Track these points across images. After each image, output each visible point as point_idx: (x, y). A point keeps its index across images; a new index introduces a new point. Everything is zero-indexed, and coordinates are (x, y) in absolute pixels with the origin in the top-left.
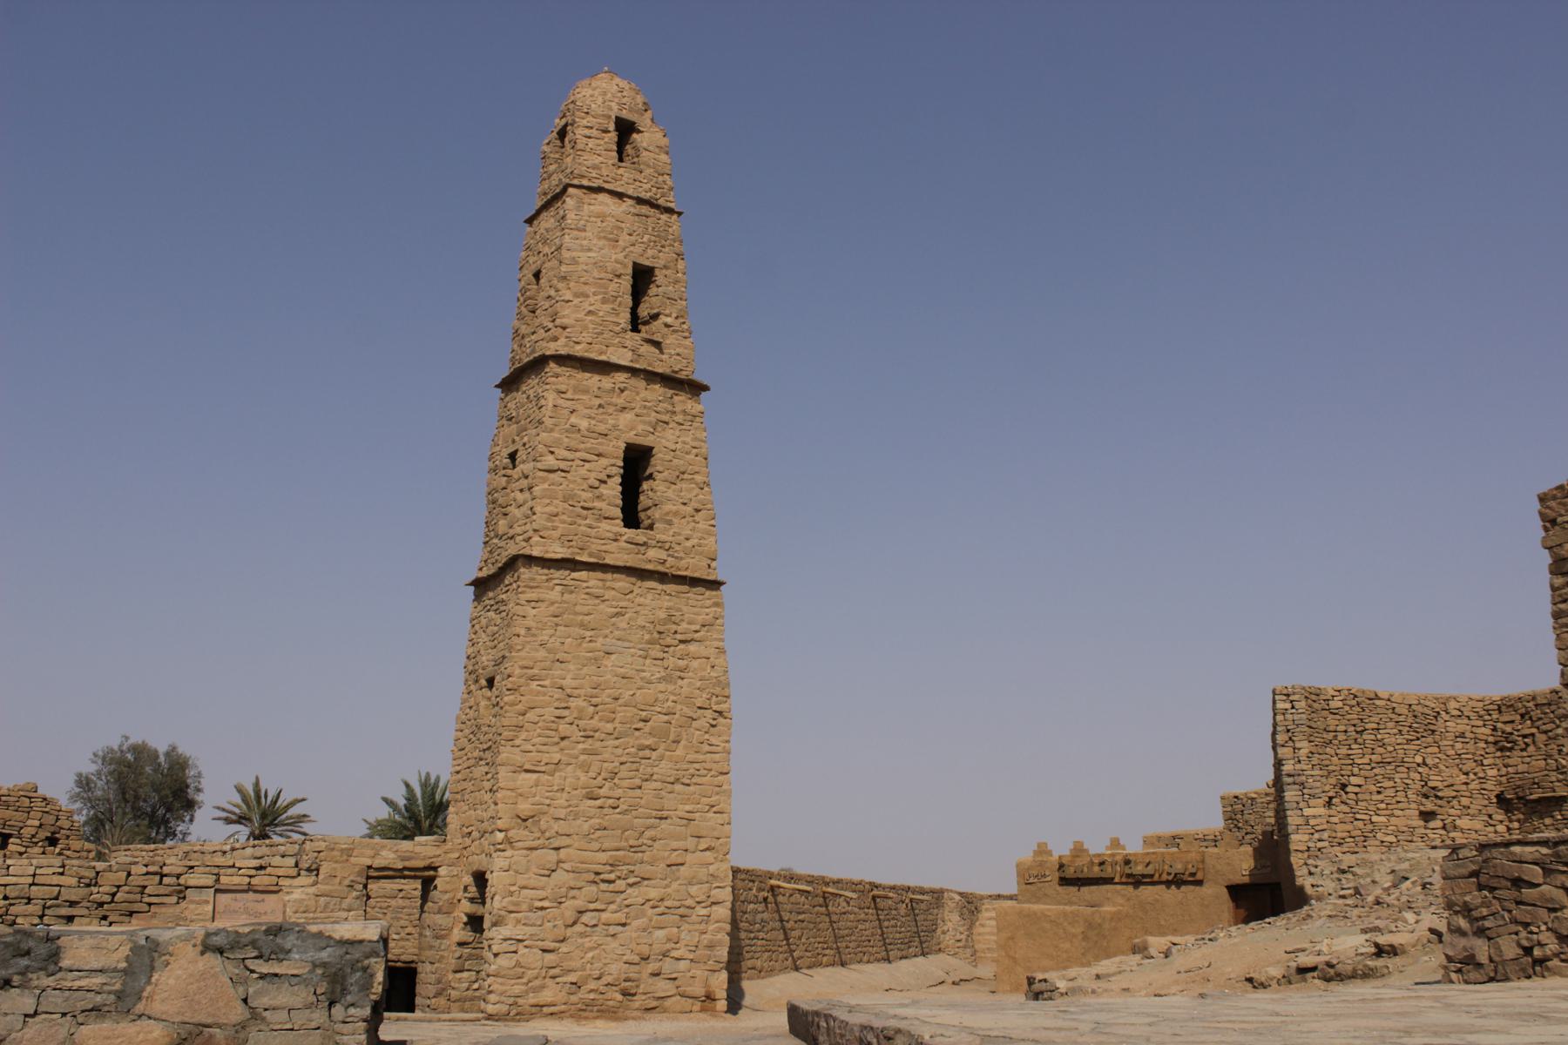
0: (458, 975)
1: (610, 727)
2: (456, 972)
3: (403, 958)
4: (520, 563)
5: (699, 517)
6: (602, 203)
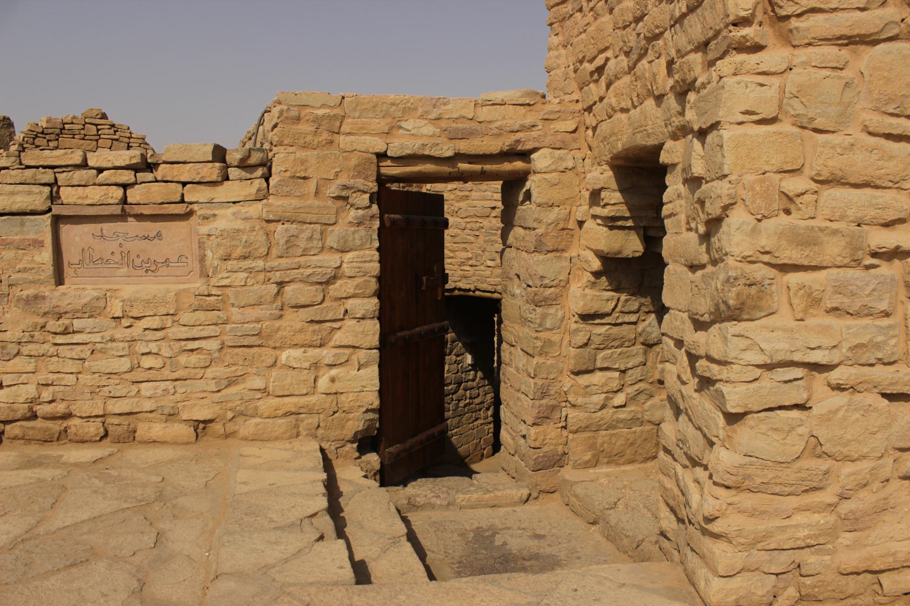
0: (583, 380)
2: (578, 373)
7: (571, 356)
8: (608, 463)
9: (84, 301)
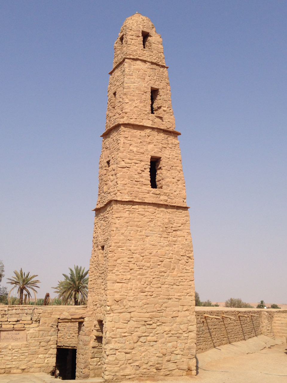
0: (93, 360)
1: (148, 264)
2: (92, 358)
3: (71, 345)
4: (113, 203)
5: (179, 183)
6: (138, 65)
7: (90, 355)
8: (97, 377)
9: (4, 346)
